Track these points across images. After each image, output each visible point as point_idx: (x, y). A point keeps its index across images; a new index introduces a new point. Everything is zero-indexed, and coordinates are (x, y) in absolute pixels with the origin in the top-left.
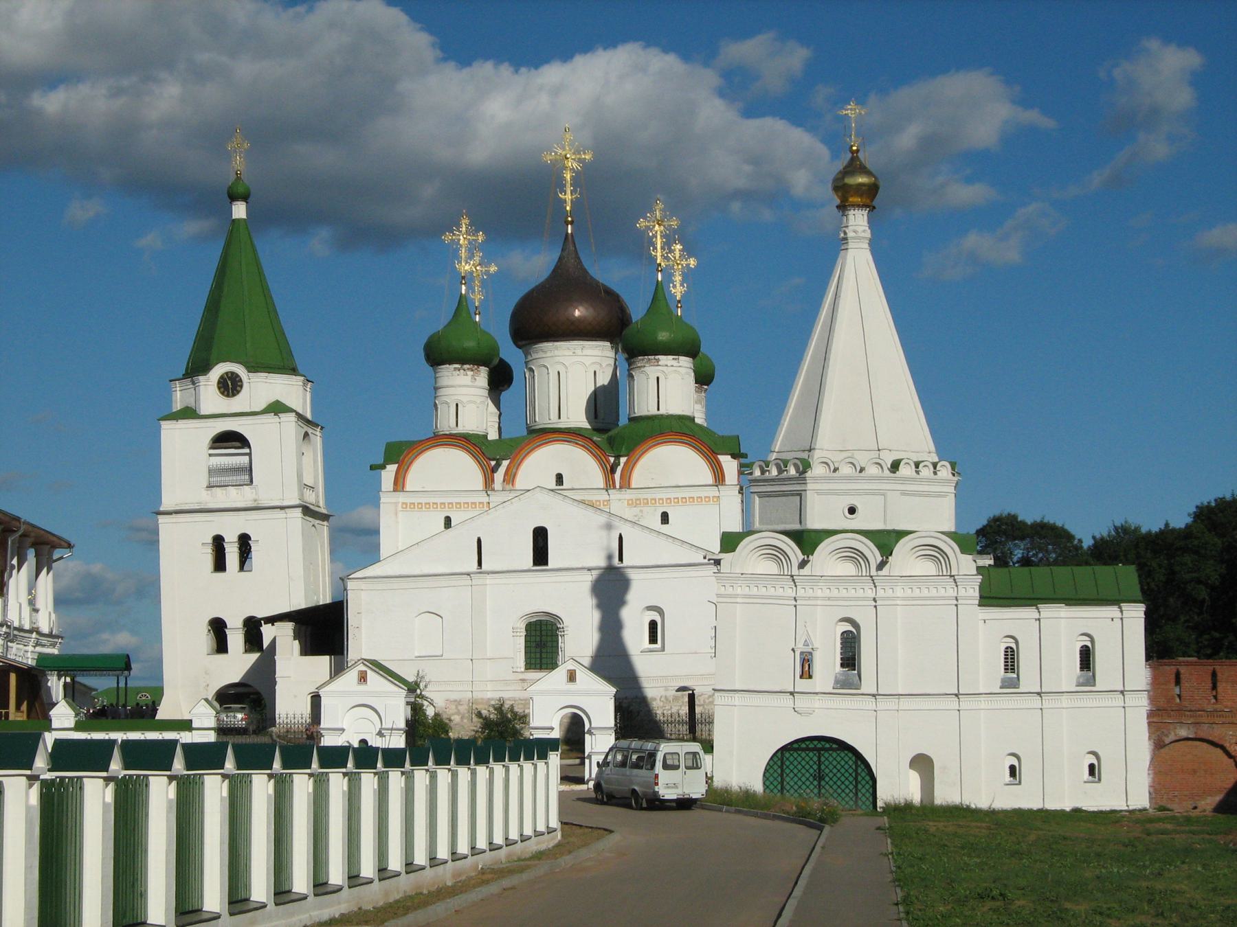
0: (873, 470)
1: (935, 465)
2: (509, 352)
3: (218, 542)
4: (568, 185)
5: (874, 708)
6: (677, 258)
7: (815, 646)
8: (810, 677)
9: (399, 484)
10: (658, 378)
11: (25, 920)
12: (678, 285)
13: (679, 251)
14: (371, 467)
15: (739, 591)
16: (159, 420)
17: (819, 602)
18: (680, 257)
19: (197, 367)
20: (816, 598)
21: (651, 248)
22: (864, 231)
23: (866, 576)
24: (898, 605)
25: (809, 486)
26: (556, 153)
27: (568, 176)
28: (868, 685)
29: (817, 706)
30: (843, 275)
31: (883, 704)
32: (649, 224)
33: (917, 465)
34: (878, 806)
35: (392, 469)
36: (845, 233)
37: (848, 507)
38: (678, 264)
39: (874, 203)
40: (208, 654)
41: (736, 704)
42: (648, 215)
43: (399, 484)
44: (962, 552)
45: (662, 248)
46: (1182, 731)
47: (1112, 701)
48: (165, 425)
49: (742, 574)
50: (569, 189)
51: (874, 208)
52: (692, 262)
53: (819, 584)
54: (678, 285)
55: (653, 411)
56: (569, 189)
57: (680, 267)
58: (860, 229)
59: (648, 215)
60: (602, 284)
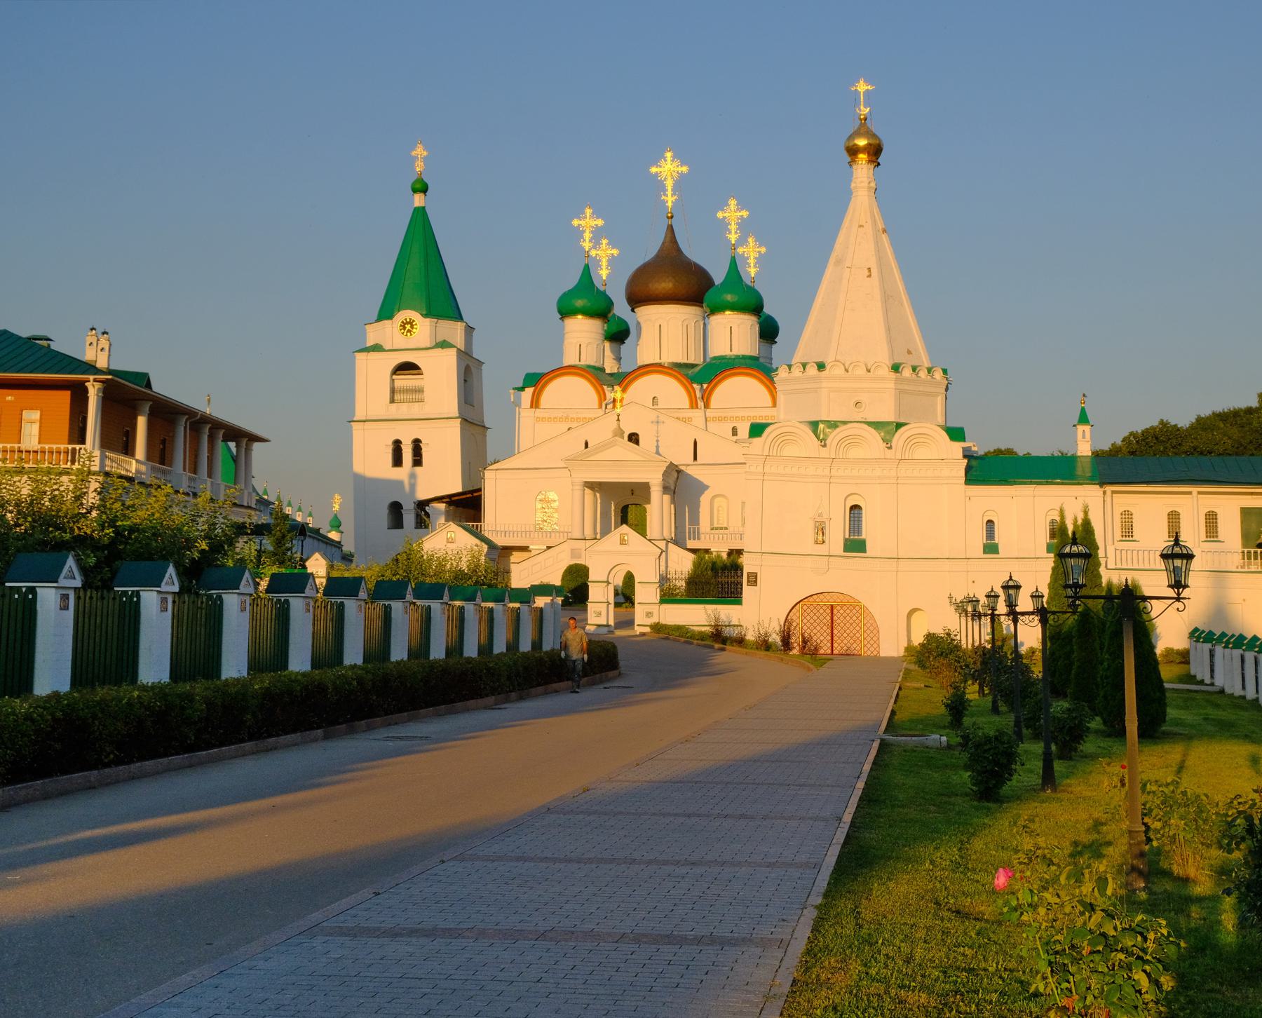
2: (621, 308)
3: (397, 446)
9: (535, 403)
11: (521, 698)
14: (856, 508)
16: (354, 352)
19: (386, 313)
35: (530, 391)
39: (879, 160)
40: (388, 529)
43: (535, 403)
46: (582, 304)
48: (360, 357)
50: (669, 192)
51: (879, 164)
56: (669, 192)
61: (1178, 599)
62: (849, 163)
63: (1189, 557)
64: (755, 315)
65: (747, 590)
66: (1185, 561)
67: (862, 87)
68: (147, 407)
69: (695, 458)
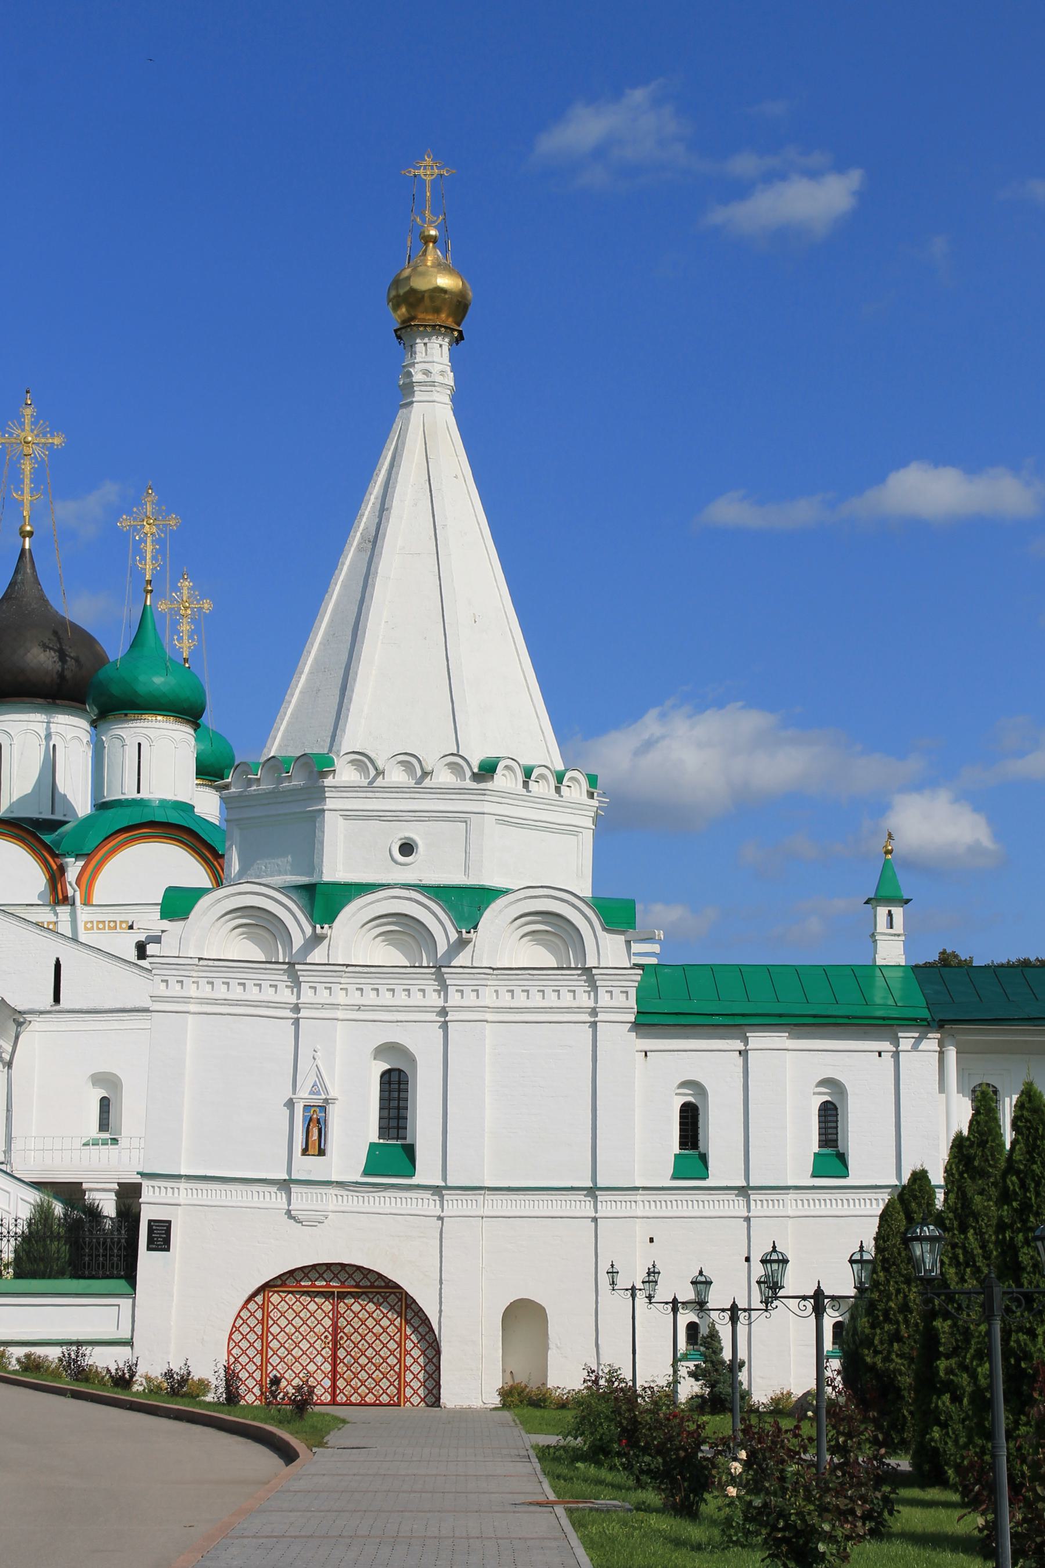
0: (444, 777)
1: (560, 778)
4: (27, 481)
5: (439, 1213)
6: (185, 599)
7: (332, 1094)
8: (321, 1152)
10: (139, 744)
12: (185, 637)
13: (188, 589)
15: (192, 991)
17: (340, 1014)
18: (189, 598)
20: (334, 1006)
21: (138, 558)
22: (442, 373)
23: (429, 967)
24: (487, 1021)
25: (329, 804)
26: (11, 434)
27: (27, 467)
28: (427, 1171)
29: (331, 1207)
30: (404, 443)
31: (454, 1204)
32: (135, 523)
33: (528, 772)
34: (632, 952)
36: (409, 375)
37: (399, 843)
38: (186, 608)
41: (182, 1201)
42: (135, 509)
44: (604, 929)
45: (154, 558)
47: (871, 1205)
49: (200, 959)
52: (206, 606)
53: (343, 980)
54: (185, 637)
55: (131, 794)
57: (189, 612)
58: (435, 369)
59: (135, 509)
60: (71, 622)
61: (766, 1310)
62: (396, 331)
63: (785, 1261)
64: (188, 722)
65: (147, 1260)
66: (781, 1265)
67: (428, 170)
68: (990, 1517)
69: (57, 999)
